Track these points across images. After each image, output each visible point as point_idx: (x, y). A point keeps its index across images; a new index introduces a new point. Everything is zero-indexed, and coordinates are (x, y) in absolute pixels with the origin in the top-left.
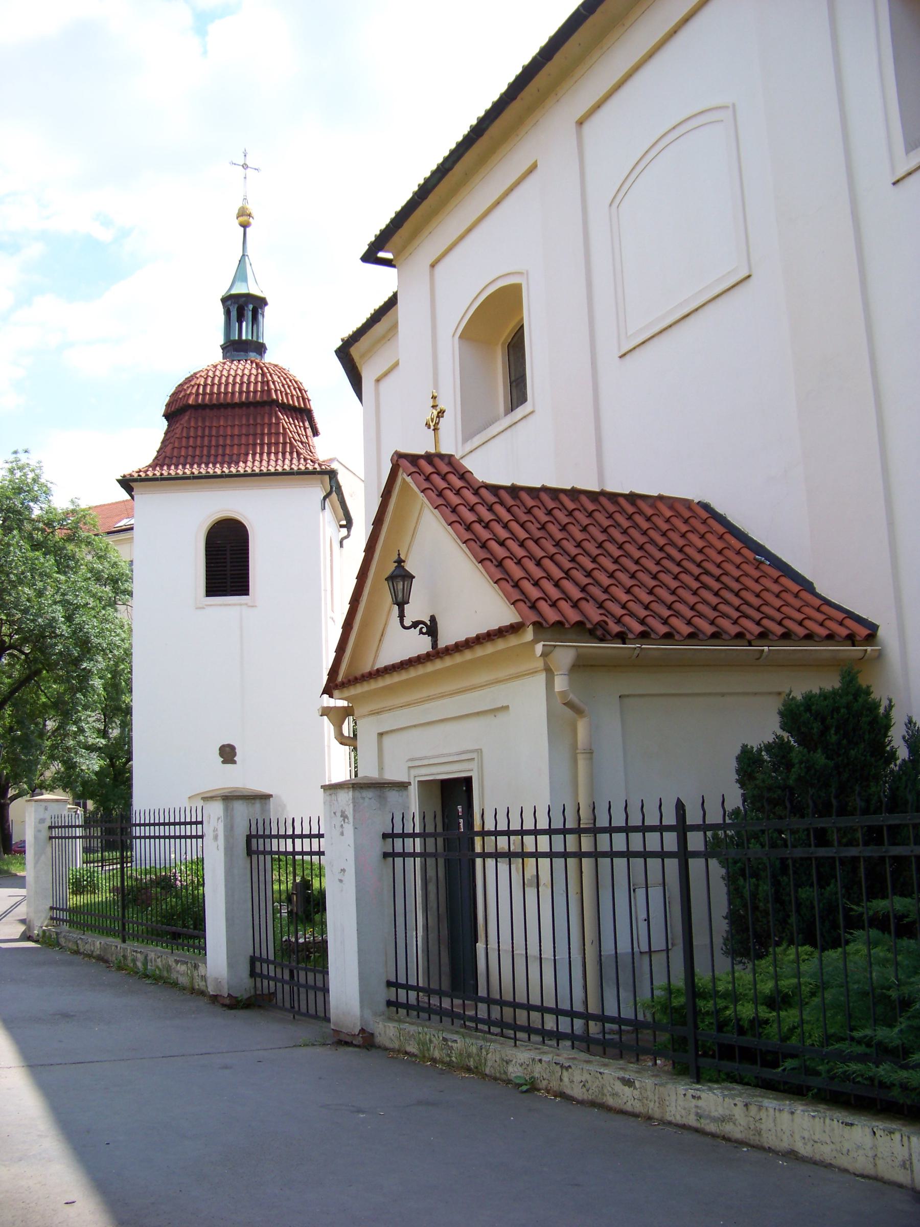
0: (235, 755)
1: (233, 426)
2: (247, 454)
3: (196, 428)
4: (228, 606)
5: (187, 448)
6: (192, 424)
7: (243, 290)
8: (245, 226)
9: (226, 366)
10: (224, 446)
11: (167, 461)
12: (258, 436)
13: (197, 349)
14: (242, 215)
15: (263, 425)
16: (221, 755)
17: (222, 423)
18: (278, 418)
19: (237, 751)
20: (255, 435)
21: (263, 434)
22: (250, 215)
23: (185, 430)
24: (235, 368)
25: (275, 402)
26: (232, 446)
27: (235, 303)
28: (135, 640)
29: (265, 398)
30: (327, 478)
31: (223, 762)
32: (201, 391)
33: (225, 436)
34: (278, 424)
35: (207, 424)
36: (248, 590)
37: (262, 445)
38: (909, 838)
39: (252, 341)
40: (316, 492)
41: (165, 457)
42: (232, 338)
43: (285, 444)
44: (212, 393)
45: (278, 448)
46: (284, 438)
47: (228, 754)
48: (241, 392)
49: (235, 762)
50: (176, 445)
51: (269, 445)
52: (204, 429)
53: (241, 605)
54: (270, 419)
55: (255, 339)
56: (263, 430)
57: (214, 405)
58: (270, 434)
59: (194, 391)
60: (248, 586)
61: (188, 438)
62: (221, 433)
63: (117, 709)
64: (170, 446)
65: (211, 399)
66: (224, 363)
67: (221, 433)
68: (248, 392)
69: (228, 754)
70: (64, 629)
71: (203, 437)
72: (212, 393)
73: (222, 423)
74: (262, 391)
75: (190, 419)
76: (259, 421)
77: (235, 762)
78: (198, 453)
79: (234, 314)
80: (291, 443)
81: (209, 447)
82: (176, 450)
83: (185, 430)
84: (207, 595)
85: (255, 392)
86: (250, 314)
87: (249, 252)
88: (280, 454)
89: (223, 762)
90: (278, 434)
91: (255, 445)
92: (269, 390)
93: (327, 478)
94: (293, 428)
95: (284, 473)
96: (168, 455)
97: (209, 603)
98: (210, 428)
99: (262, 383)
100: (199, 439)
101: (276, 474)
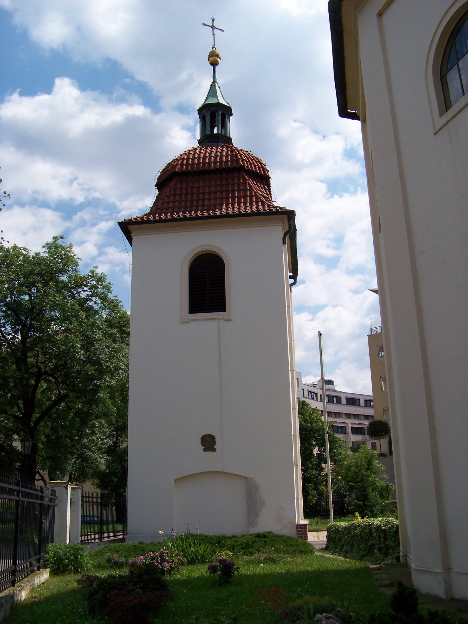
0: (214, 443)
1: (210, 187)
2: (222, 205)
3: (181, 189)
4: (208, 322)
5: (174, 202)
6: (178, 186)
7: (215, 101)
8: (214, 64)
9: (202, 151)
10: (204, 200)
11: (158, 211)
12: (230, 192)
13: (182, 138)
14: (212, 56)
15: (233, 185)
16: (203, 444)
17: (201, 184)
18: (245, 179)
19: (217, 440)
20: (227, 192)
21: (233, 191)
22: (218, 56)
23: (172, 190)
24: (209, 152)
25: (242, 168)
26: (209, 200)
27: (208, 110)
28: (131, 372)
29: (235, 165)
30: (286, 217)
31: (205, 450)
32: (185, 162)
33: (204, 194)
34: (245, 184)
35: (190, 185)
36: (225, 309)
37: (233, 198)
38: (328, 511)
39: (221, 135)
40: (277, 231)
41: (157, 209)
42: (206, 133)
43: (251, 196)
44: (193, 164)
45: (246, 200)
46: (251, 193)
47: (208, 443)
48: (215, 162)
49: (214, 450)
50: (166, 200)
51: (239, 198)
52: (187, 189)
53: (219, 319)
54: (239, 180)
55: (223, 133)
56: (234, 187)
57: (195, 171)
58: (239, 191)
59: (179, 163)
60: (225, 305)
61: (175, 196)
62: (201, 191)
63: (121, 429)
64: (161, 202)
65: (192, 168)
66: (201, 149)
67: (201, 191)
68: (221, 162)
69: (208, 443)
70: (81, 354)
71: (186, 195)
72: (193, 164)
73: (201, 184)
74: (232, 161)
75: (176, 183)
76: (230, 182)
77: (214, 450)
78: (182, 205)
79: (208, 118)
80: (256, 196)
81: (192, 201)
82: (165, 204)
83: (172, 190)
84: (190, 313)
85: (227, 161)
86: (220, 117)
87: (218, 80)
88: (248, 204)
89: (205, 450)
90: (245, 190)
91: (227, 198)
92: (238, 160)
93: (286, 217)
94: (256, 187)
95: (252, 214)
96: (159, 207)
97: (190, 318)
98: (192, 188)
99: (232, 156)
100: (183, 196)
101: (246, 214)
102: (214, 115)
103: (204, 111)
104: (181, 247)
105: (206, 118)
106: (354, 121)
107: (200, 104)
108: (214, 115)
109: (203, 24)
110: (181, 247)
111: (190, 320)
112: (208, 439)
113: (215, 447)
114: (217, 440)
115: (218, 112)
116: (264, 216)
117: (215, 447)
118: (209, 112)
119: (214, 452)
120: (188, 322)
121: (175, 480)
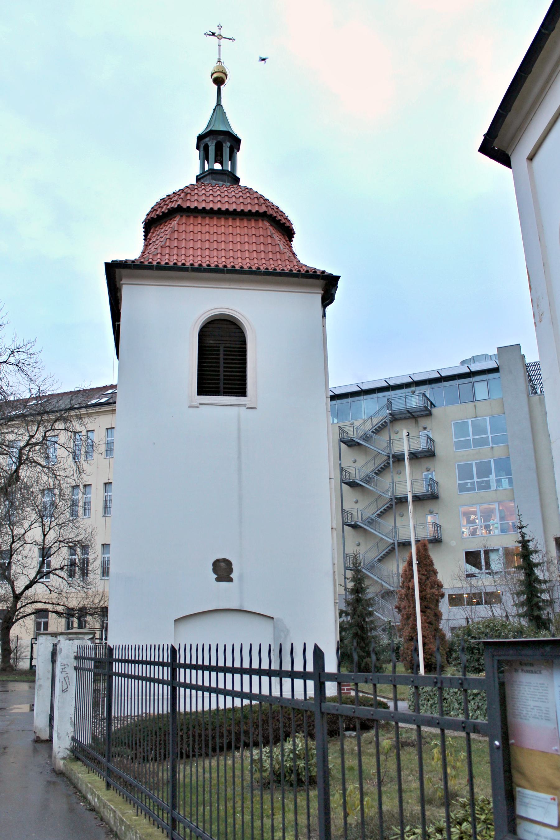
0: (231, 571)
16: (215, 571)
27: (213, 139)
47: (223, 570)
69: (223, 570)
77: (231, 580)
86: (228, 150)
89: (218, 580)
102: (219, 143)
103: (207, 139)
104: (176, 314)
105: (210, 148)
106: (482, 138)
107: (201, 129)
108: (219, 143)
109: (205, 34)
110: (176, 314)
111: (200, 404)
112: (223, 564)
113: (231, 576)
114: (234, 567)
115: (226, 144)
116: (302, 279)
117: (231, 576)
118: (215, 142)
119: (230, 583)
120: (197, 407)
121: (175, 621)
